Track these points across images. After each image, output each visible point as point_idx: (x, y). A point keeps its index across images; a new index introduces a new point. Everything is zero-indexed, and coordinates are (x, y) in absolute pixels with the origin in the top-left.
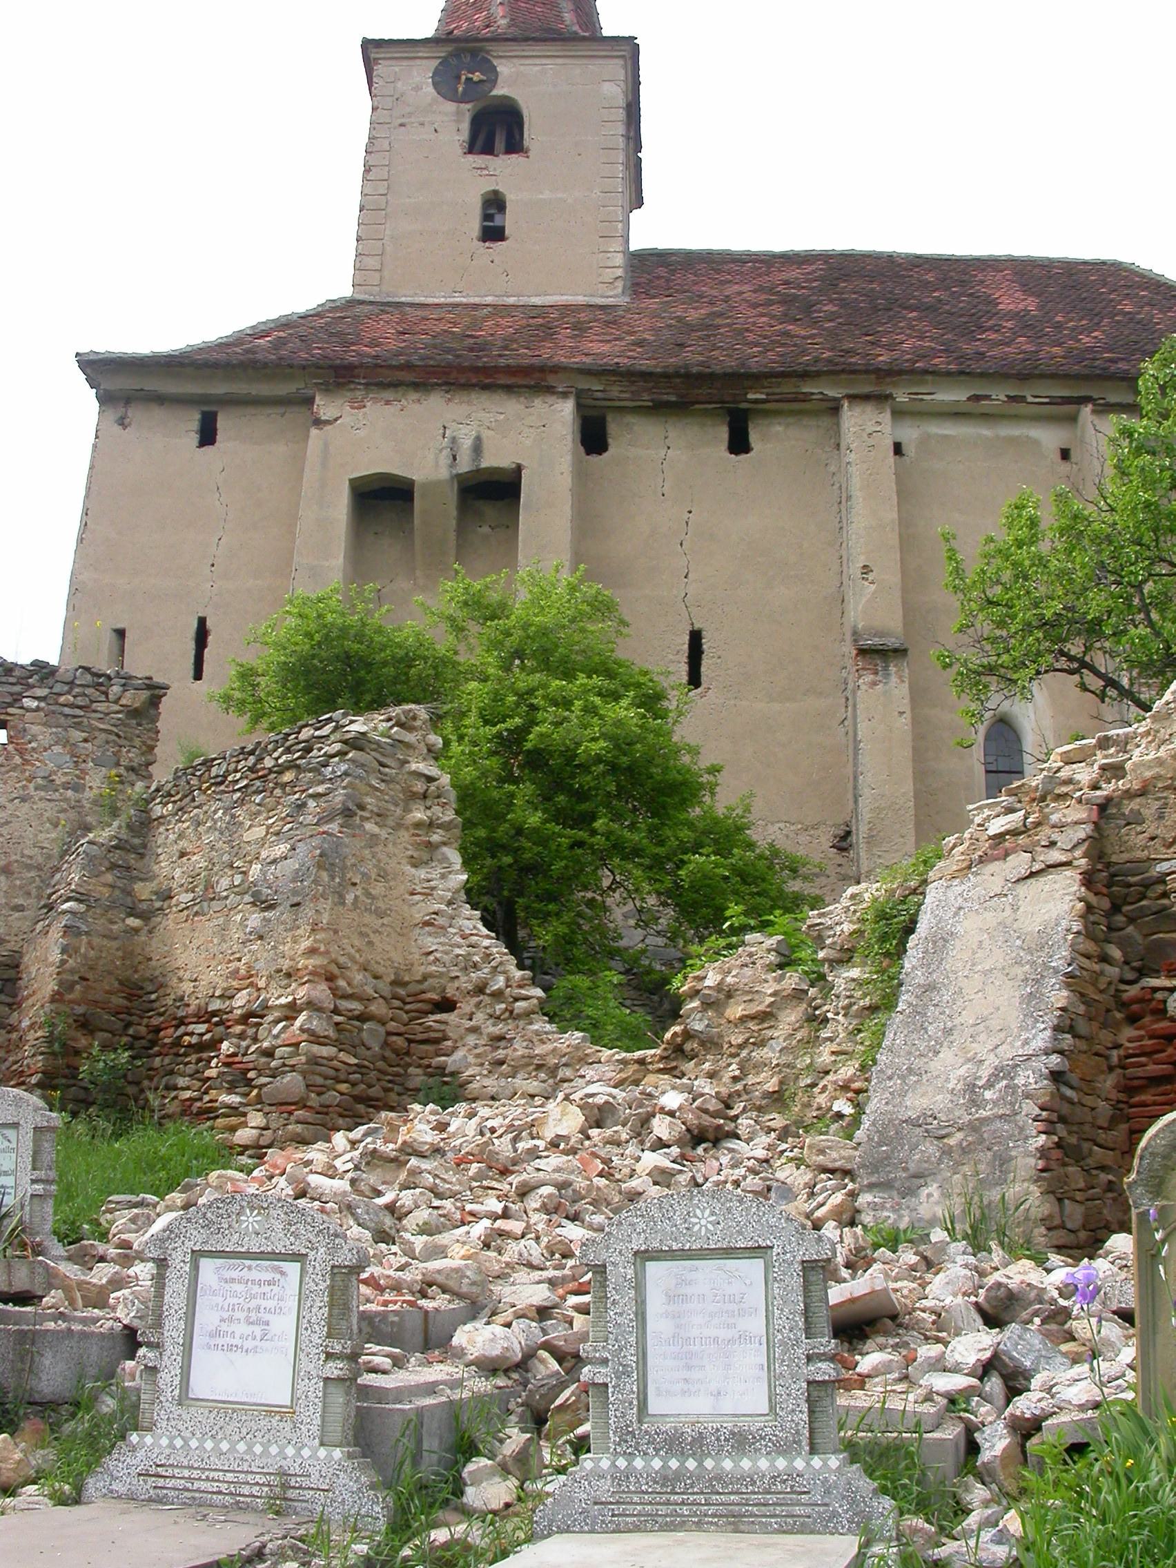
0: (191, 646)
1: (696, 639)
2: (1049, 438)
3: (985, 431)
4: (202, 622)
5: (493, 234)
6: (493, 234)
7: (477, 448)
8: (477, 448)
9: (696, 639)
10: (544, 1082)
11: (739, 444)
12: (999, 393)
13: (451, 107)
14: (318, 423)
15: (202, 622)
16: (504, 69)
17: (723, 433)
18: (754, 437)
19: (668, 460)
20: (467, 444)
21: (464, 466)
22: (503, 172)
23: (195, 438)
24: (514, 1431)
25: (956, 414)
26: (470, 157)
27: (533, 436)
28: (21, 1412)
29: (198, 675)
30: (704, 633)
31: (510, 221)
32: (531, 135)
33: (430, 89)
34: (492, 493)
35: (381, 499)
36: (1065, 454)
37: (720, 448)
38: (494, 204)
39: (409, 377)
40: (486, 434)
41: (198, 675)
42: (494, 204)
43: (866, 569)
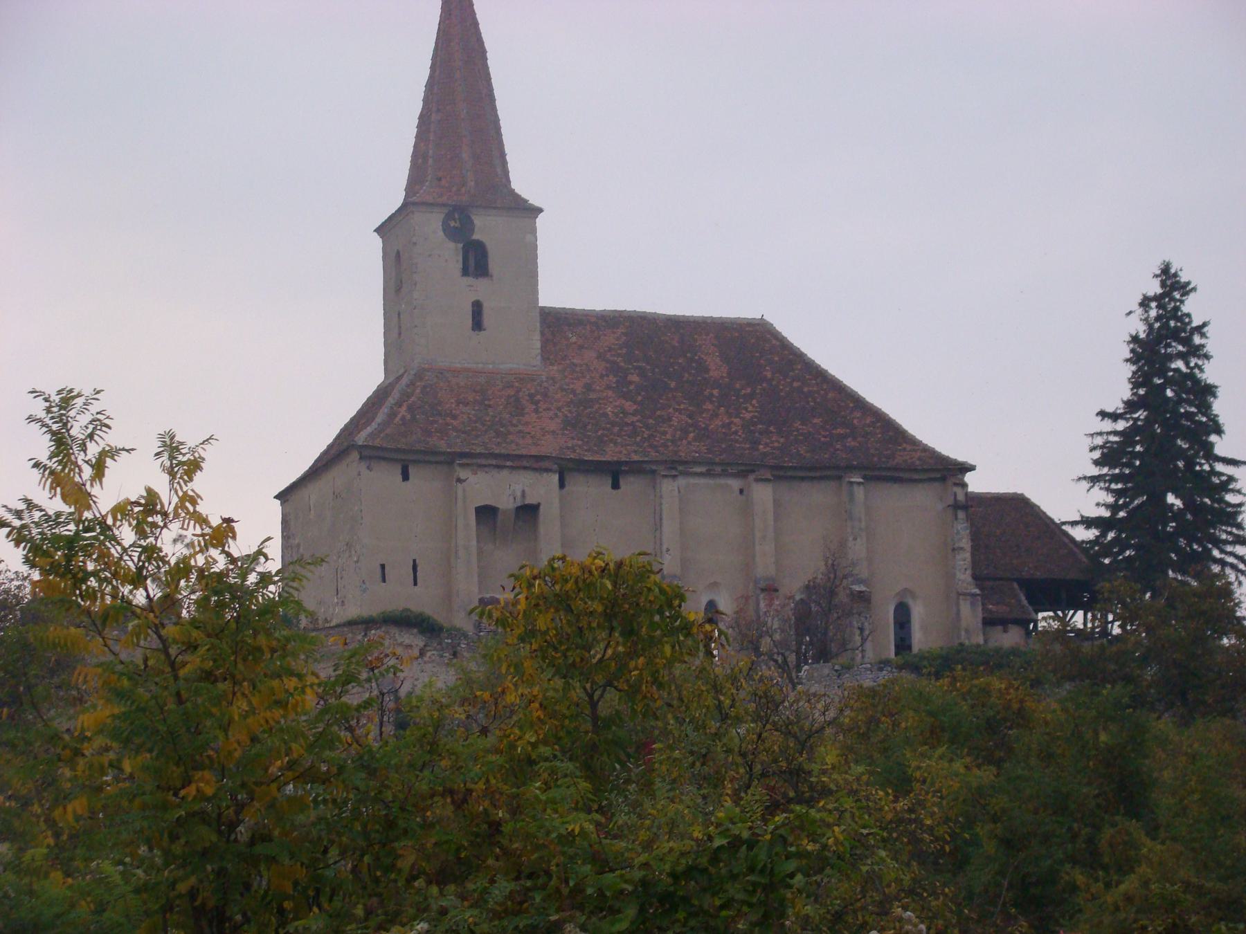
2: (735, 484)
3: (711, 482)
4: (414, 561)
5: (478, 325)
6: (478, 325)
7: (523, 494)
8: (523, 494)
10: (313, 674)
11: (616, 486)
12: (718, 469)
13: (452, 245)
15: (414, 561)
16: (478, 221)
19: (588, 490)
20: (519, 494)
22: (480, 289)
23: (400, 478)
24: (1161, 725)
26: (465, 279)
27: (543, 488)
28: (1094, 752)
29: (415, 584)
31: (487, 319)
32: (494, 265)
33: (441, 233)
34: (528, 512)
35: (486, 513)
36: (741, 491)
37: (609, 488)
38: (477, 308)
40: (526, 489)
41: (415, 584)
42: (477, 308)
43: (668, 550)
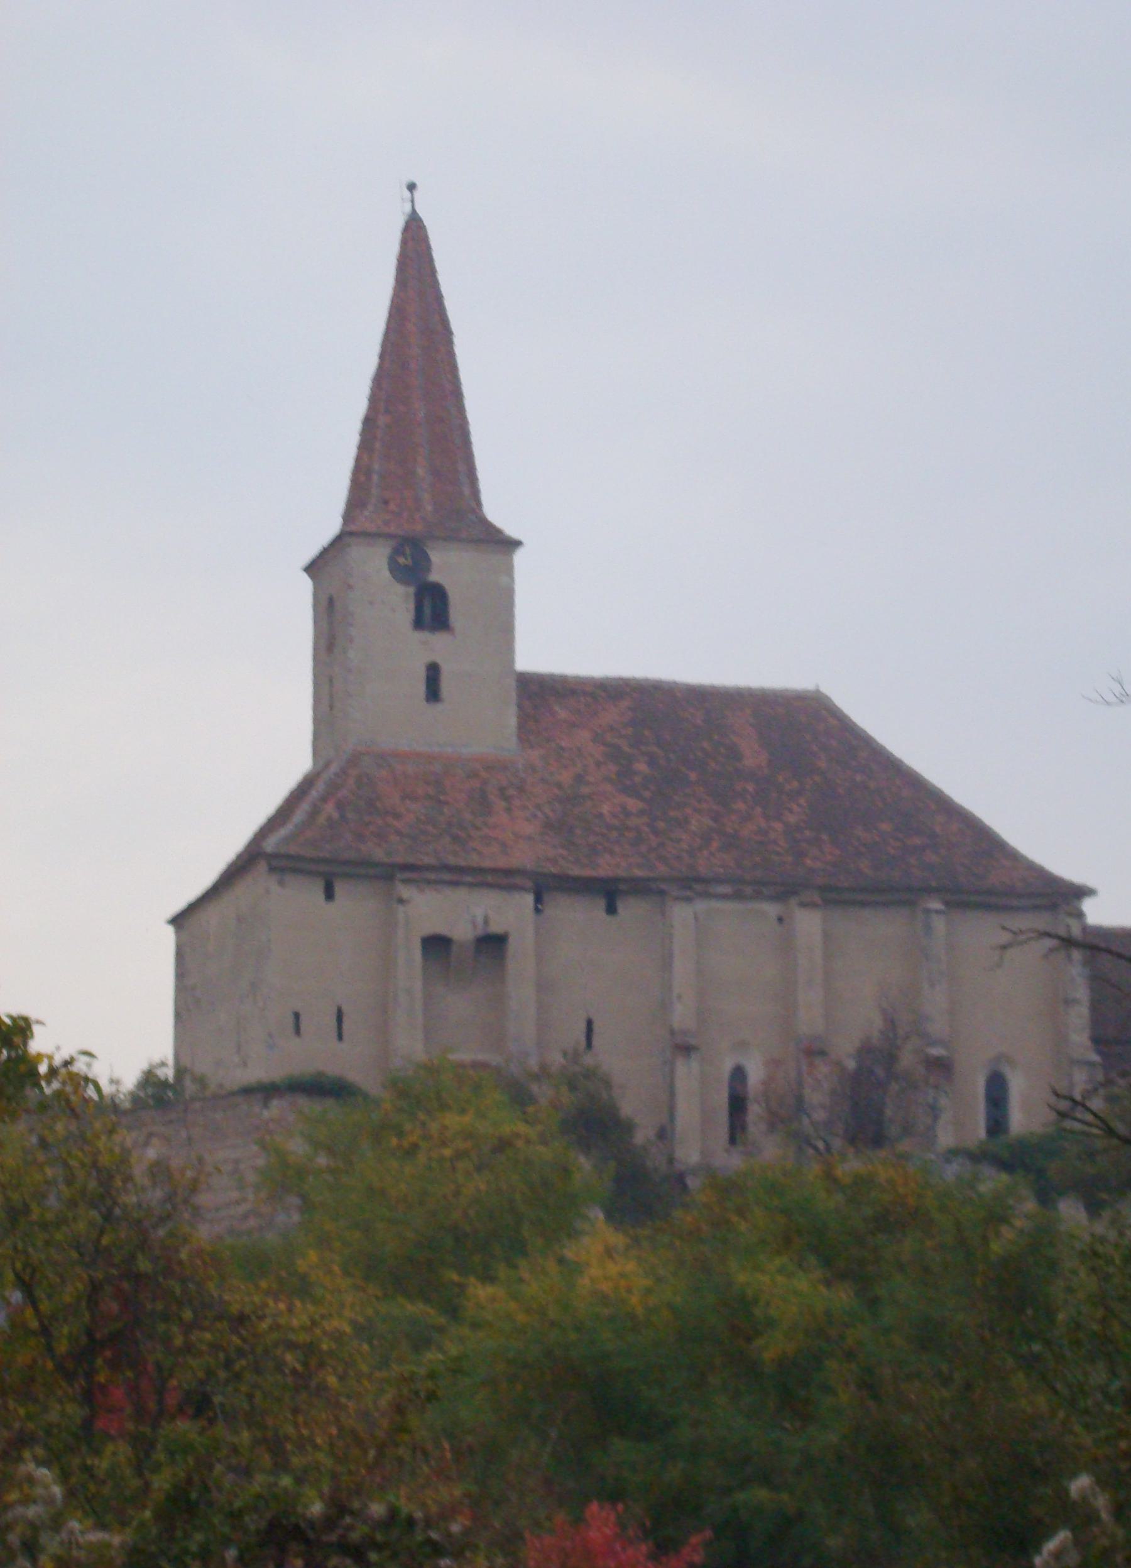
0: (334, 1022)
1: (590, 1023)
2: (772, 909)
7: (486, 921)
8: (486, 921)
9: (590, 1023)
14: (401, 901)
16: (435, 557)
17: (602, 903)
18: (620, 906)
19: (576, 915)
20: (480, 920)
21: (480, 932)
25: (724, 897)
27: (510, 913)
30: (36, 1029)
32: (456, 615)
34: (492, 944)
35: (436, 946)
36: (780, 920)
38: (433, 674)
39: (447, 876)
42: (433, 674)
